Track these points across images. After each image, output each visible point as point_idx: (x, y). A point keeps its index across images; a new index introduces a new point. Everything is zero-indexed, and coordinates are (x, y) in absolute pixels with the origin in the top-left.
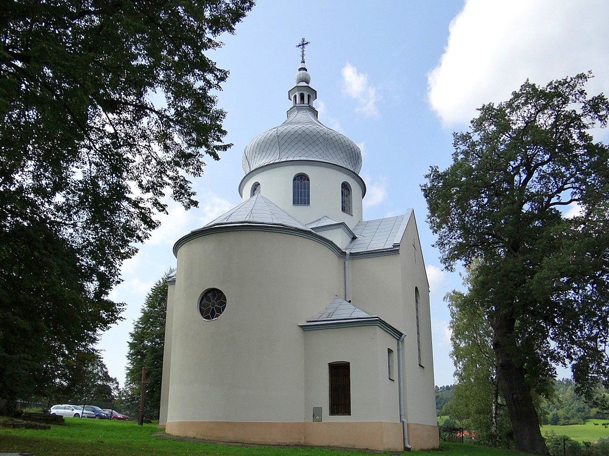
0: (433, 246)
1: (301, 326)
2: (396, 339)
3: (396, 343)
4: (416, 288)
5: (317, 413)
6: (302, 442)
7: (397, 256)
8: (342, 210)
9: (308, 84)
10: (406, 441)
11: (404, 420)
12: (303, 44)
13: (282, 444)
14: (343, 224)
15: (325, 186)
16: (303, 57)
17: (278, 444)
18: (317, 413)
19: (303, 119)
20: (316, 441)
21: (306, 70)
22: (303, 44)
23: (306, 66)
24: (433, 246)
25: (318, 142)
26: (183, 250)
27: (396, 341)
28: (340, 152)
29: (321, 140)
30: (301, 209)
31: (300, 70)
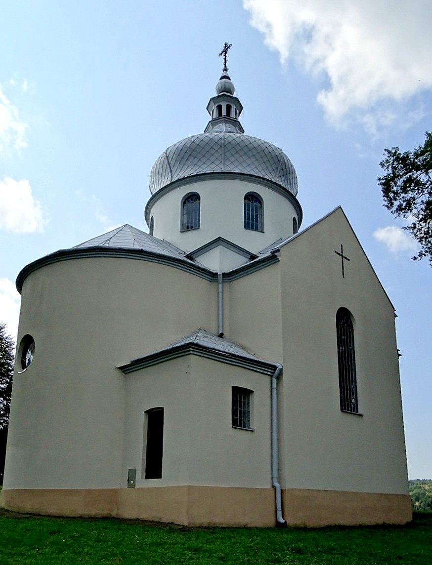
0: (415, 259)
1: (120, 368)
2: (269, 375)
3: (269, 381)
4: (344, 318)
5: (131, 476)
6: (114, 514)
7: (223, 272)
8: (245, 227)
9: (231, 94)
10: (280, 513)
11: (277, 484)
12: (227, 48)
13: (85, 517)
14: (219, 239)
15: (273, 206)
16: (225, 65)
17: (78, 516)
18: (131, 476)
19: (223, 130)
20: (128, 513)
21: (230, 79)
22: (227, 48)
23: (229, 73)
24: (415, 259)
25: (213, 151)
26: (27, 285)
27: (268, 378)
28: (245, 157)
29: (246, 150)
30: (191, 234)
31: (222, 78)
